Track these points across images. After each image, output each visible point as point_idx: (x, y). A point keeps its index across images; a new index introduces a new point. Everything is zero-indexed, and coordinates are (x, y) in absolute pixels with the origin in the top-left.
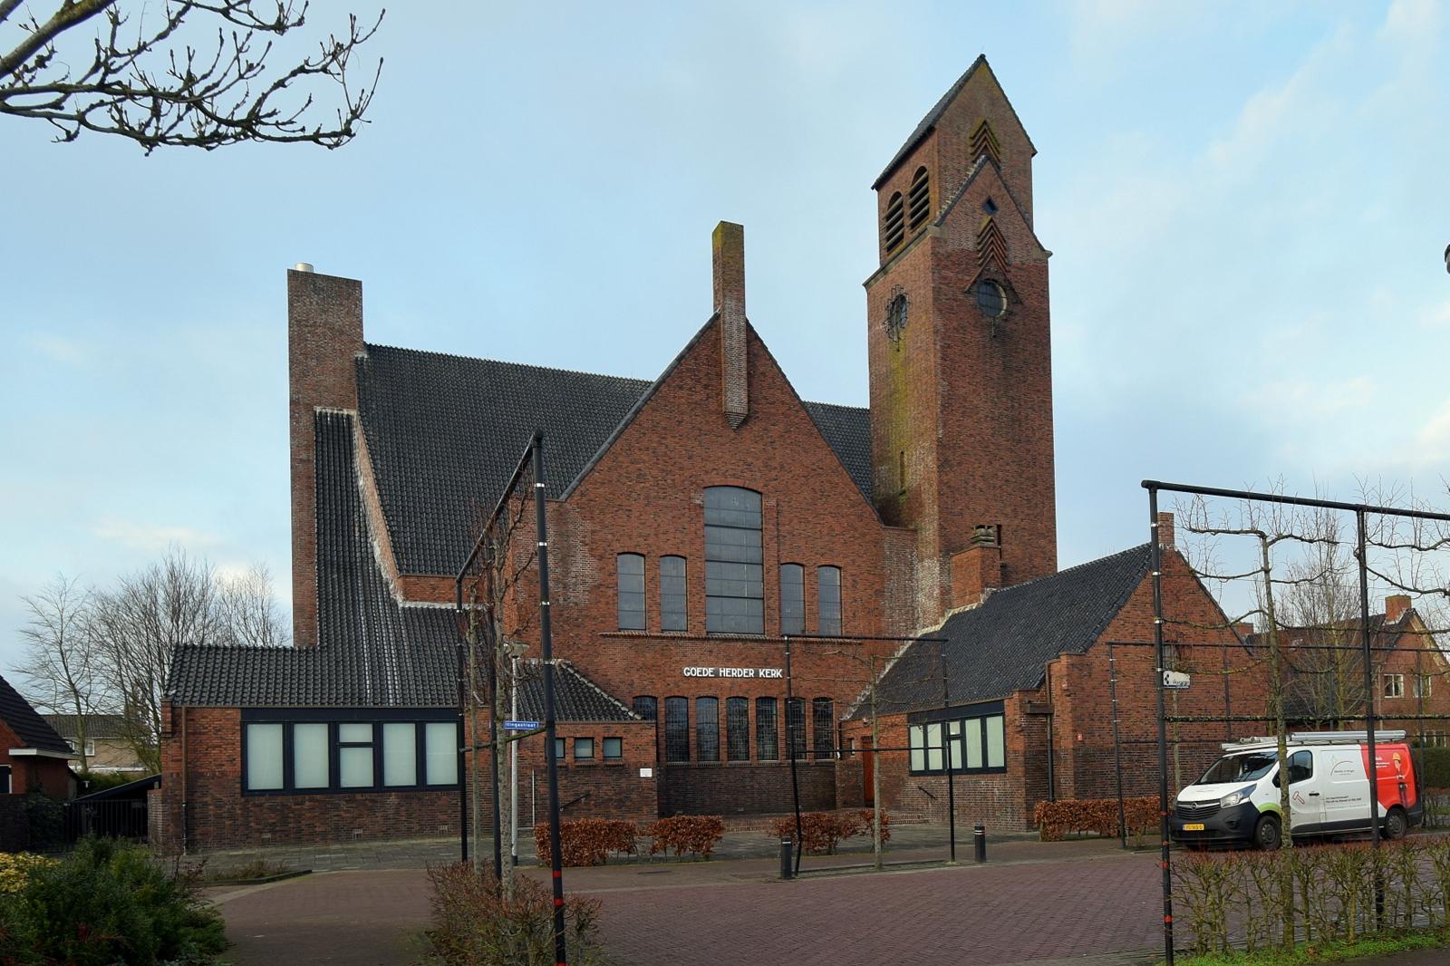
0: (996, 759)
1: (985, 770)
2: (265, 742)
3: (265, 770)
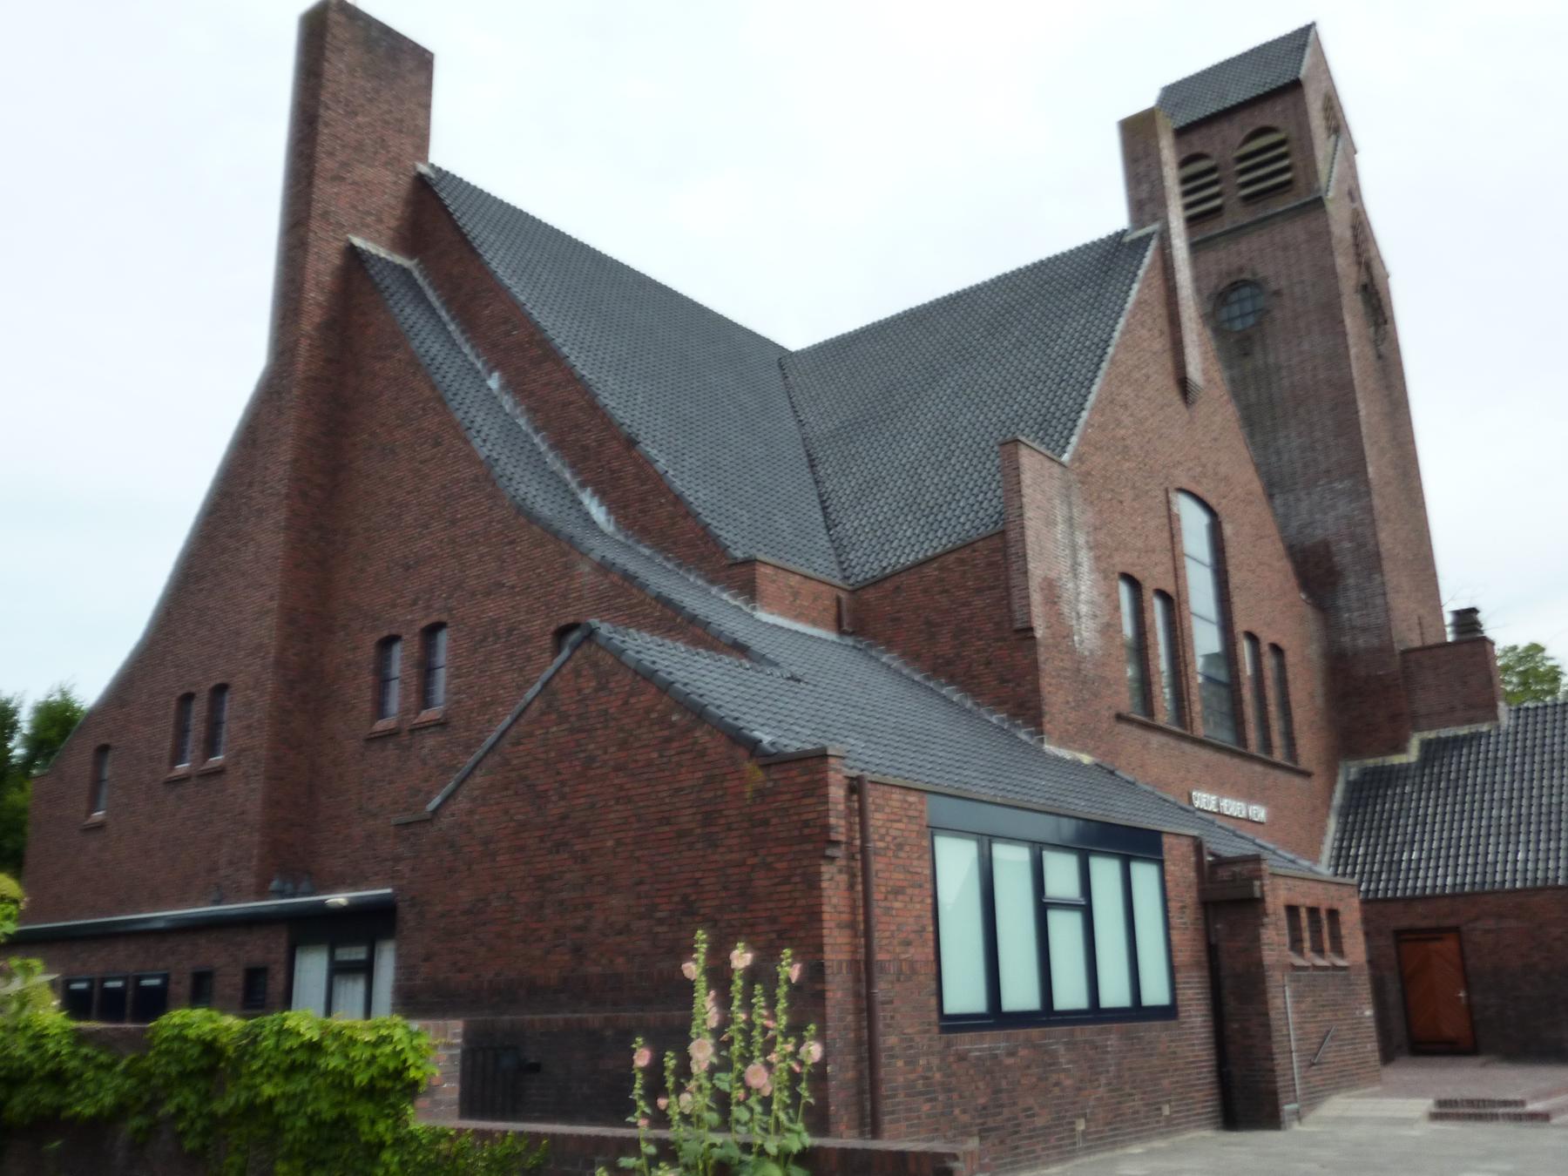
0: (1155, 992)
1: (1137, 1011)
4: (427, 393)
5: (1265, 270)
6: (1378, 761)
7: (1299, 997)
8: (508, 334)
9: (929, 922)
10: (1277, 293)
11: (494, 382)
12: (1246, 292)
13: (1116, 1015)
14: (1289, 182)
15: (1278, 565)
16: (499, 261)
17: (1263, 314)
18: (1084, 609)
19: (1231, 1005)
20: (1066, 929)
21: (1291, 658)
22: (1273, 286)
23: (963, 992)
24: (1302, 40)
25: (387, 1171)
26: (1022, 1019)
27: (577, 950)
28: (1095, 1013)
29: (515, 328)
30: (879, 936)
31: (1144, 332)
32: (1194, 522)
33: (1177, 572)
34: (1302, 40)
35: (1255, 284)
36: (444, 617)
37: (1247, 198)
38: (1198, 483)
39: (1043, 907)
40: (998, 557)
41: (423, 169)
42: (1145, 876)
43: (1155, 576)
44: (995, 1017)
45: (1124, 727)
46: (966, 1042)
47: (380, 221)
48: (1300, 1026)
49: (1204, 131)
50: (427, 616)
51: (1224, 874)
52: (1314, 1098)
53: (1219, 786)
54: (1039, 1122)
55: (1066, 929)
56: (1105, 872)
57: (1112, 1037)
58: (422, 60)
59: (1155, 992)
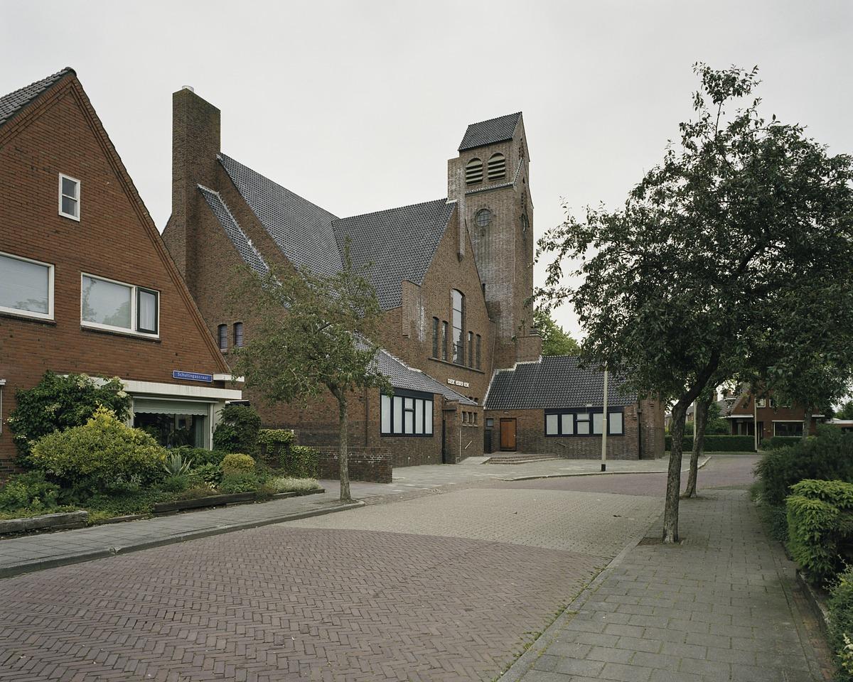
0: (429, 431)
1: (424, 435)
2: (552, 420)
3: (552, 429)
4: (232, 248)
5: (492, 207)
6: (505, 370)
7: (463, 433)
8: (254, 227)
9: (379, 414)
10: (495, 216)
11: (250, 243)
12: (486, 212)
13: (419, 435)
14: (504, 176)
15: (482, 310)
16: (248, 195)
17: (490, 222)
18: (422, 329)
19: (447, 434)
20: (409, 416)
21: (482, 339)
22: (494, 213)
23: (386, 429)
24: (515, 120)
25: (852, 317)
26: (398, 435)
27: (300, 417)
28: (414, 435)
29: (256, 225)
30: (369, 416)
31: (448, 239)
32: (457, 298)
33: (450, 316)
34: (515, 120)
35: (489, 211)
36: (241, 321)
37: (490, 178)
38: (460, 286)
39: (404, 410)
40: (400, 314)
41: (219, 157)
42: (429, 404)
43: (442, 318)
44: (392, 434)
45: (431, 361)
46: (386, 439)
47: (206, 178)
48: (462, 440)
49: (480, 150)
50: (235, 320)
51: (448, 404)
52: (464, 457)
53: (455, 378)
54: (400, 457)
55: (409, 416)
56: (419, 403)
57: (417, 440)
58: (216, 112)
59: (429, 431)
